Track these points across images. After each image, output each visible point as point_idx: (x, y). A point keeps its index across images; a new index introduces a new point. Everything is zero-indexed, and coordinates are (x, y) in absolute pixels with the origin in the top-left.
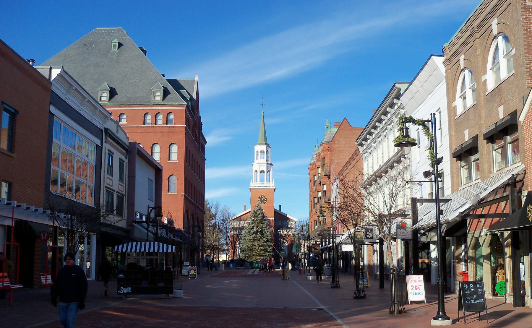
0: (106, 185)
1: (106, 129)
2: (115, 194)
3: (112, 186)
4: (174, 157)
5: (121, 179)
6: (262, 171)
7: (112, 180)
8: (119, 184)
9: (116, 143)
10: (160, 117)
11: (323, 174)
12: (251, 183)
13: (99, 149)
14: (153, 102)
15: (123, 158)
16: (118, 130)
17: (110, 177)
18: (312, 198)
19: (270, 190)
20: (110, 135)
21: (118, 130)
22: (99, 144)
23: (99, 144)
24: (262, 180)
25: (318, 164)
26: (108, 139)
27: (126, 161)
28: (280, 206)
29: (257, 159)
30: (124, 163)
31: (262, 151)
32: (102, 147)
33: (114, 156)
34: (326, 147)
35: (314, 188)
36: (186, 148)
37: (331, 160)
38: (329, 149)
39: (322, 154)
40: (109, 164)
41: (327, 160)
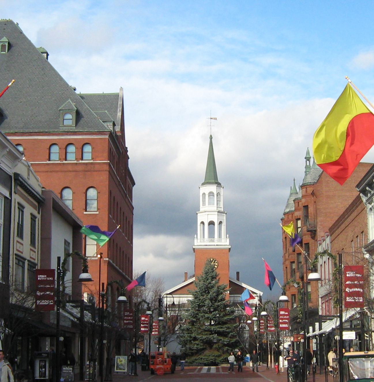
0: (16, 252)
1: (16, 175)
2: (26, 263)
3: (22, 253)
4: (93, 207)
5: (33, 243)
6: (211, 223)
7: (22, 244)
8: (31, 250)
9: (30, 195)
10: (72, 149)
11: (305, 229)
12: (196, 240)
13: (8, 202)
14: (62, 129)
15: (35, 213)
16: (29, 175)
17: (20, 240)
18: (288, 263)
19: (222, 250)
20: (21, 182)
21: (29, 175)
22: (8, 195)
23: (8, 195)
24: (211, 235)
25: (298, 214)
26: (19, 188)
27: (39, 216)
28: (238, 273)
29: (204, 204)
30: (37, 220)
31: (211, 194)
32: (11, 200)
33: (25, 210)
34: (310, 190)
35: (291, 249)
36: (110, 193)
37: (316, 210)
38: (313, 194)
39: (303, 200)
40: (18, 223)
41: (311, 209)
